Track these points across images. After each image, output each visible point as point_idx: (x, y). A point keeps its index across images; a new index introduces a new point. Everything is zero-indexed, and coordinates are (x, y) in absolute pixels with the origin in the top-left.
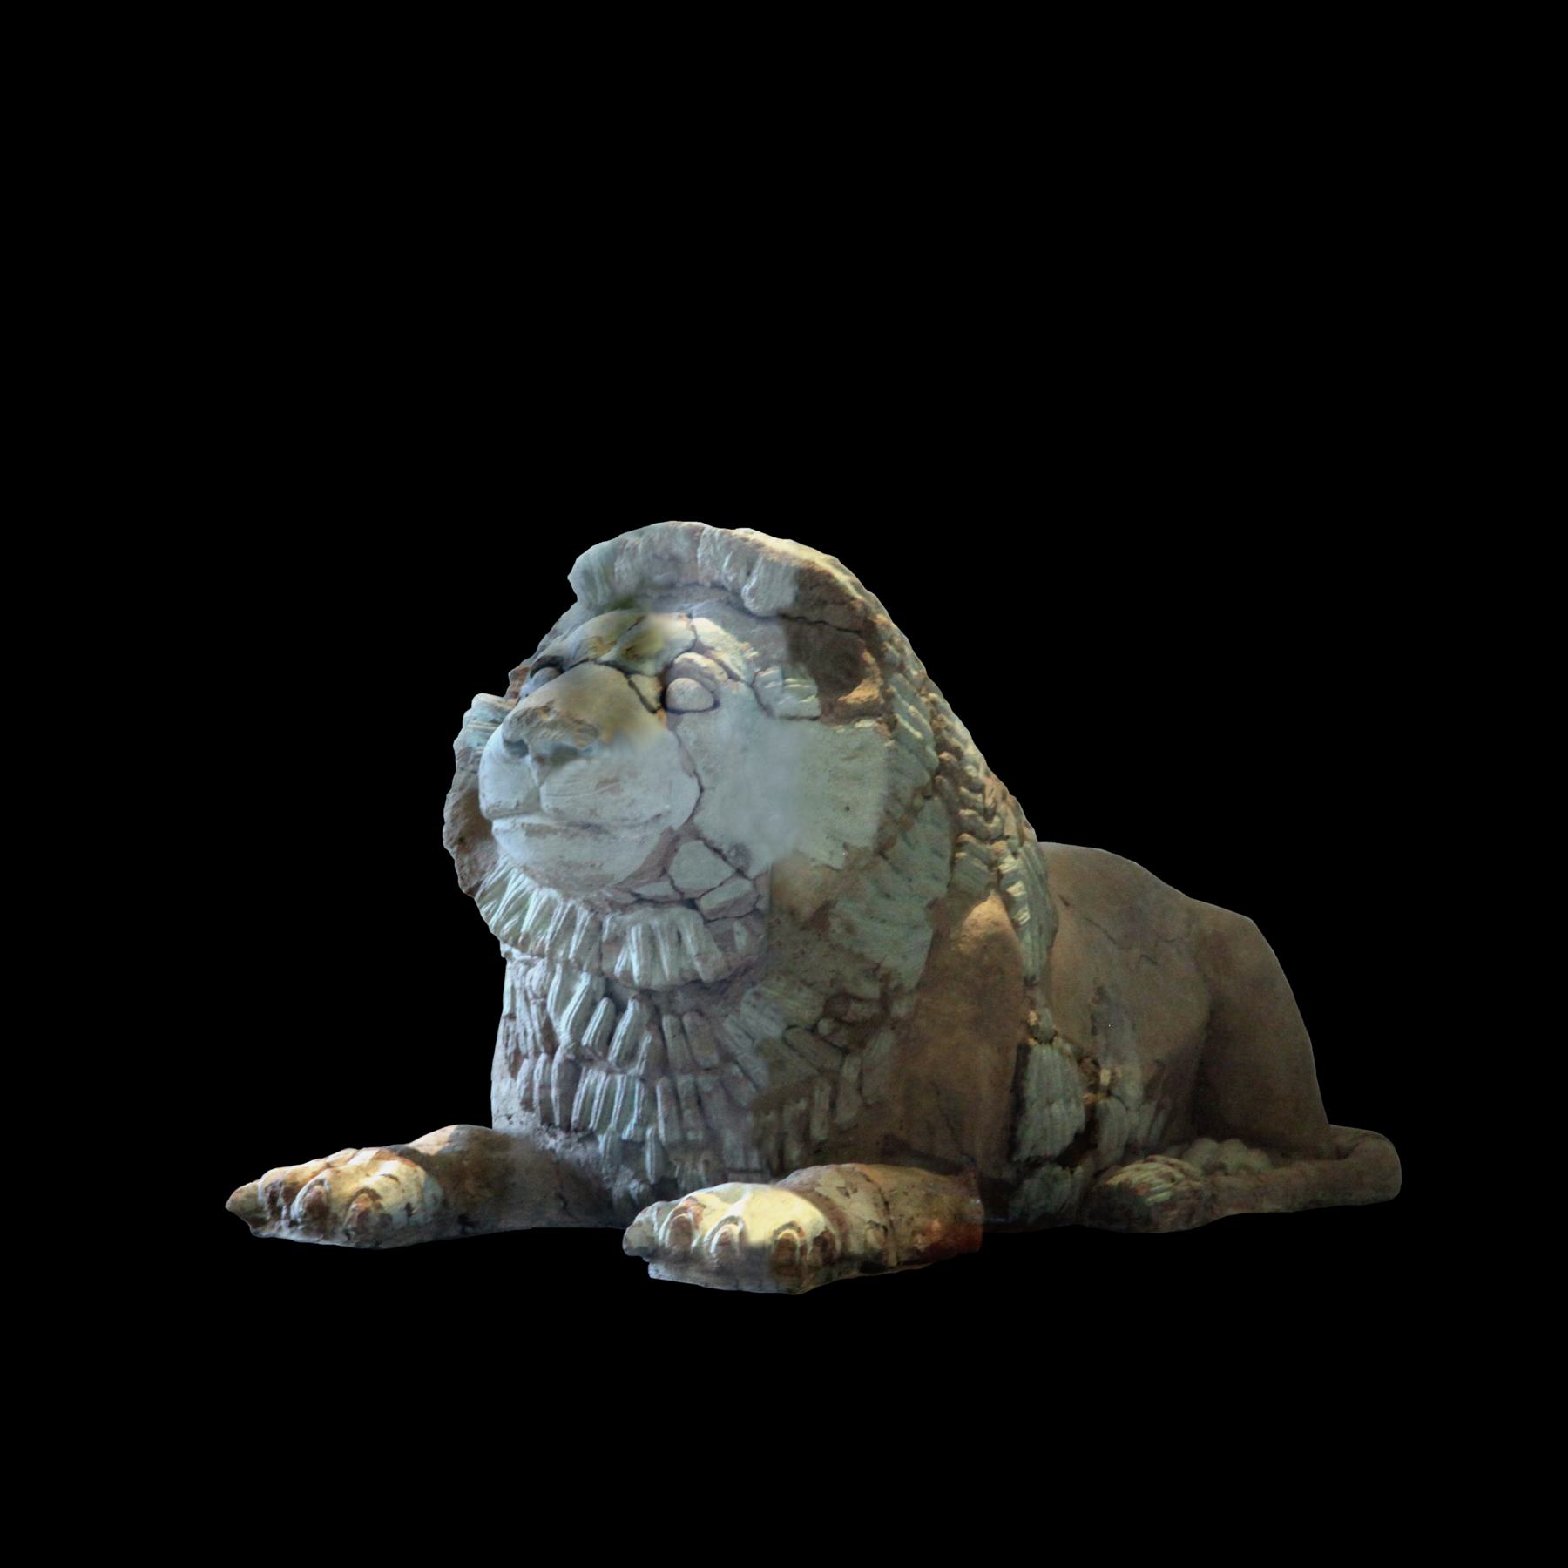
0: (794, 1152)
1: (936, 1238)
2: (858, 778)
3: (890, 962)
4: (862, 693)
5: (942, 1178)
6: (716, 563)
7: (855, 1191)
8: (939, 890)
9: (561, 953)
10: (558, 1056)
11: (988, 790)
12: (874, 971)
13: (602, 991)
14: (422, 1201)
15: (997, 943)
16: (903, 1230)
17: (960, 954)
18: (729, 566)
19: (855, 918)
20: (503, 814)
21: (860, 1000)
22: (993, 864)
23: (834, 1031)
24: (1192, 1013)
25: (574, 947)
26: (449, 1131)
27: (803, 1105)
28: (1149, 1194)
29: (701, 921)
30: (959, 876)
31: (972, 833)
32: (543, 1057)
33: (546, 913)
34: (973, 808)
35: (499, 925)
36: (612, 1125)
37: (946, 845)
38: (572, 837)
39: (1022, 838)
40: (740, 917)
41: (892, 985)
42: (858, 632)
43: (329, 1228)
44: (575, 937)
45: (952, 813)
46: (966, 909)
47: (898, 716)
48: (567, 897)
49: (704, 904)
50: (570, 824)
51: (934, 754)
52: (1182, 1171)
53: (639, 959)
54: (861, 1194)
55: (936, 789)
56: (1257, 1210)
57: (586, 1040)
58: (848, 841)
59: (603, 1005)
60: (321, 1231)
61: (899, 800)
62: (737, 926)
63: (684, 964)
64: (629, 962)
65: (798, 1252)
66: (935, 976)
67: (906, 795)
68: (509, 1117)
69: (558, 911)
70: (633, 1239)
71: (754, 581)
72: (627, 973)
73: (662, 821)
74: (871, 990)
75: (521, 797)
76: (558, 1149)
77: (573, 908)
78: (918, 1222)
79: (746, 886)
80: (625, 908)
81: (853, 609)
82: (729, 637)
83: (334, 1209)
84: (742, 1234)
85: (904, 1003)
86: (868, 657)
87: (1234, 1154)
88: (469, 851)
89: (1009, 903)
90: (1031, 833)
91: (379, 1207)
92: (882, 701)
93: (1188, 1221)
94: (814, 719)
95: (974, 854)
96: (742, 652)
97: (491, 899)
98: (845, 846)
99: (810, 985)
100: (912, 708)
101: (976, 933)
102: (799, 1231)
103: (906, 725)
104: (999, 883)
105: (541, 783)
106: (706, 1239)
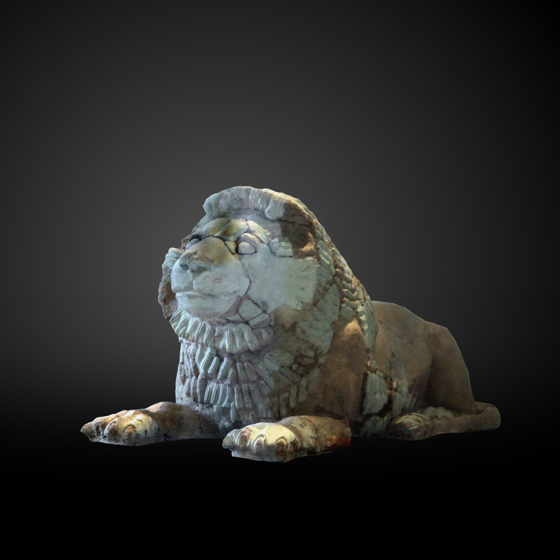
0: (284, 411)
1: (334, 442)
2: (306, 278)
3: (318, 343)
4: (308, 248)
5: (336, 421)
6: (256, 201)
7: (305, 425)
8: (335, 318)
9: (200, 340)
10: (199, 377)
11: (353, 282)
12: (312, 347)
13: (215, 354)
14: (151, 429)
15: (356, 337)
16: (322, 439)
17: (343, 341)
18: (260, 202)
19: (305, 328)
20: (180, 291)
21: (307, 357)
22: (355, 309)
23: (298, 368)
24: (426, 362)
25: (205, 338)
26: (160, 404)
27: (287, 395)
28: (410, 426)
29: (250, 329)
30: (343, 313)
31: (347, 297)
32: (194, 377)
33: (195, 326)
34: (348, 289)
35: (178, 331)
36: (219, 402)
37: (338, 302)
38: (204, 299)
39: (365, 299)
40: (264, 328)
41: (319, 352)
42: (306, 226)
43: (118, 438)
44: (205, 335)
45: (340, 290)
46: (345, 325)
47: (321, 256)
48: (202, 320)
49: (251, 323)
50: (204, 294)
51: (334, 269)
52: (422, 418)
53: (228, 342)
54: (307, 427)
55: (334, 282)
56: (449, 432)
57: (209, 371)
58: (303, 300)
59: (215, 359)
60: (115, 440)
61: (321, 286)
62: (263, 331)
63: (244, 344)
64: (224, 344)
65: (285, 447)
66: (334, 349)
67: (324, 284)
68: (182, 399)
69: (199, 325)
70: (226, 442)
71: (269, 207)
72: (224, 348)
73: (236, 293)
74: (311, 353)
75: (186, 285)
76: (199, 410)
77: (204, 324)
78: (328, 436)
79: (266, 316)
80: (223, 324)
81: (305, 217)
82: (260, 227)
83: (119, 432)
84: (265, 441)
85: (323, 358)
86: (310, 235)
87: (441, 412)
88: (167, 304)
89: (360, 323)
90: (368, 297)
91: (135, 431)
92: (315, 251)
93: (424, 436)
94: (291, 257)
95: (348, 305)
96: (265, 233)
97: (175, 321)
98: (302, 302)
99: (289, 352)
100: (326, 253)
101: (349, 333)
102: (285, 440)
103: (324, 259)
104: (357, 316)
105: (193, 280)
106: (252, 443)
